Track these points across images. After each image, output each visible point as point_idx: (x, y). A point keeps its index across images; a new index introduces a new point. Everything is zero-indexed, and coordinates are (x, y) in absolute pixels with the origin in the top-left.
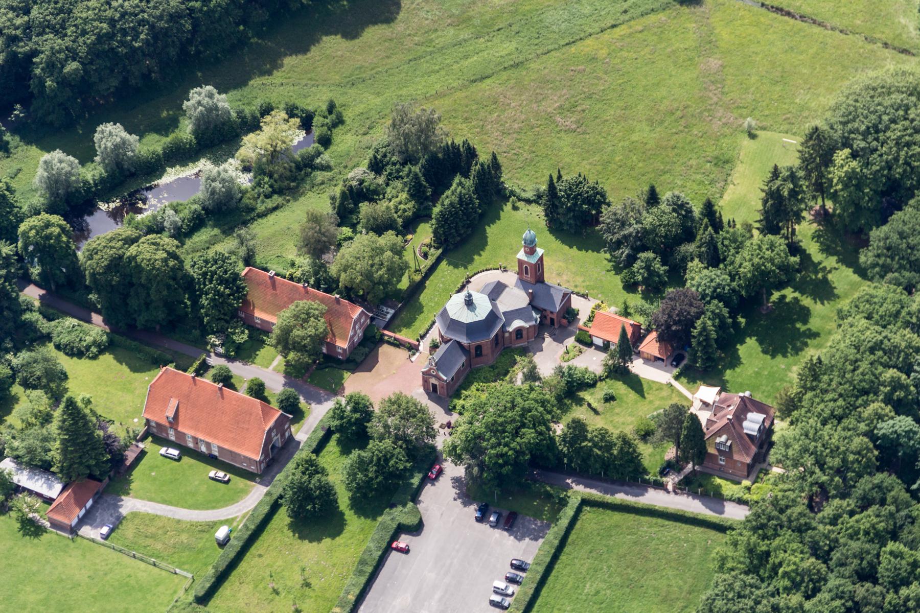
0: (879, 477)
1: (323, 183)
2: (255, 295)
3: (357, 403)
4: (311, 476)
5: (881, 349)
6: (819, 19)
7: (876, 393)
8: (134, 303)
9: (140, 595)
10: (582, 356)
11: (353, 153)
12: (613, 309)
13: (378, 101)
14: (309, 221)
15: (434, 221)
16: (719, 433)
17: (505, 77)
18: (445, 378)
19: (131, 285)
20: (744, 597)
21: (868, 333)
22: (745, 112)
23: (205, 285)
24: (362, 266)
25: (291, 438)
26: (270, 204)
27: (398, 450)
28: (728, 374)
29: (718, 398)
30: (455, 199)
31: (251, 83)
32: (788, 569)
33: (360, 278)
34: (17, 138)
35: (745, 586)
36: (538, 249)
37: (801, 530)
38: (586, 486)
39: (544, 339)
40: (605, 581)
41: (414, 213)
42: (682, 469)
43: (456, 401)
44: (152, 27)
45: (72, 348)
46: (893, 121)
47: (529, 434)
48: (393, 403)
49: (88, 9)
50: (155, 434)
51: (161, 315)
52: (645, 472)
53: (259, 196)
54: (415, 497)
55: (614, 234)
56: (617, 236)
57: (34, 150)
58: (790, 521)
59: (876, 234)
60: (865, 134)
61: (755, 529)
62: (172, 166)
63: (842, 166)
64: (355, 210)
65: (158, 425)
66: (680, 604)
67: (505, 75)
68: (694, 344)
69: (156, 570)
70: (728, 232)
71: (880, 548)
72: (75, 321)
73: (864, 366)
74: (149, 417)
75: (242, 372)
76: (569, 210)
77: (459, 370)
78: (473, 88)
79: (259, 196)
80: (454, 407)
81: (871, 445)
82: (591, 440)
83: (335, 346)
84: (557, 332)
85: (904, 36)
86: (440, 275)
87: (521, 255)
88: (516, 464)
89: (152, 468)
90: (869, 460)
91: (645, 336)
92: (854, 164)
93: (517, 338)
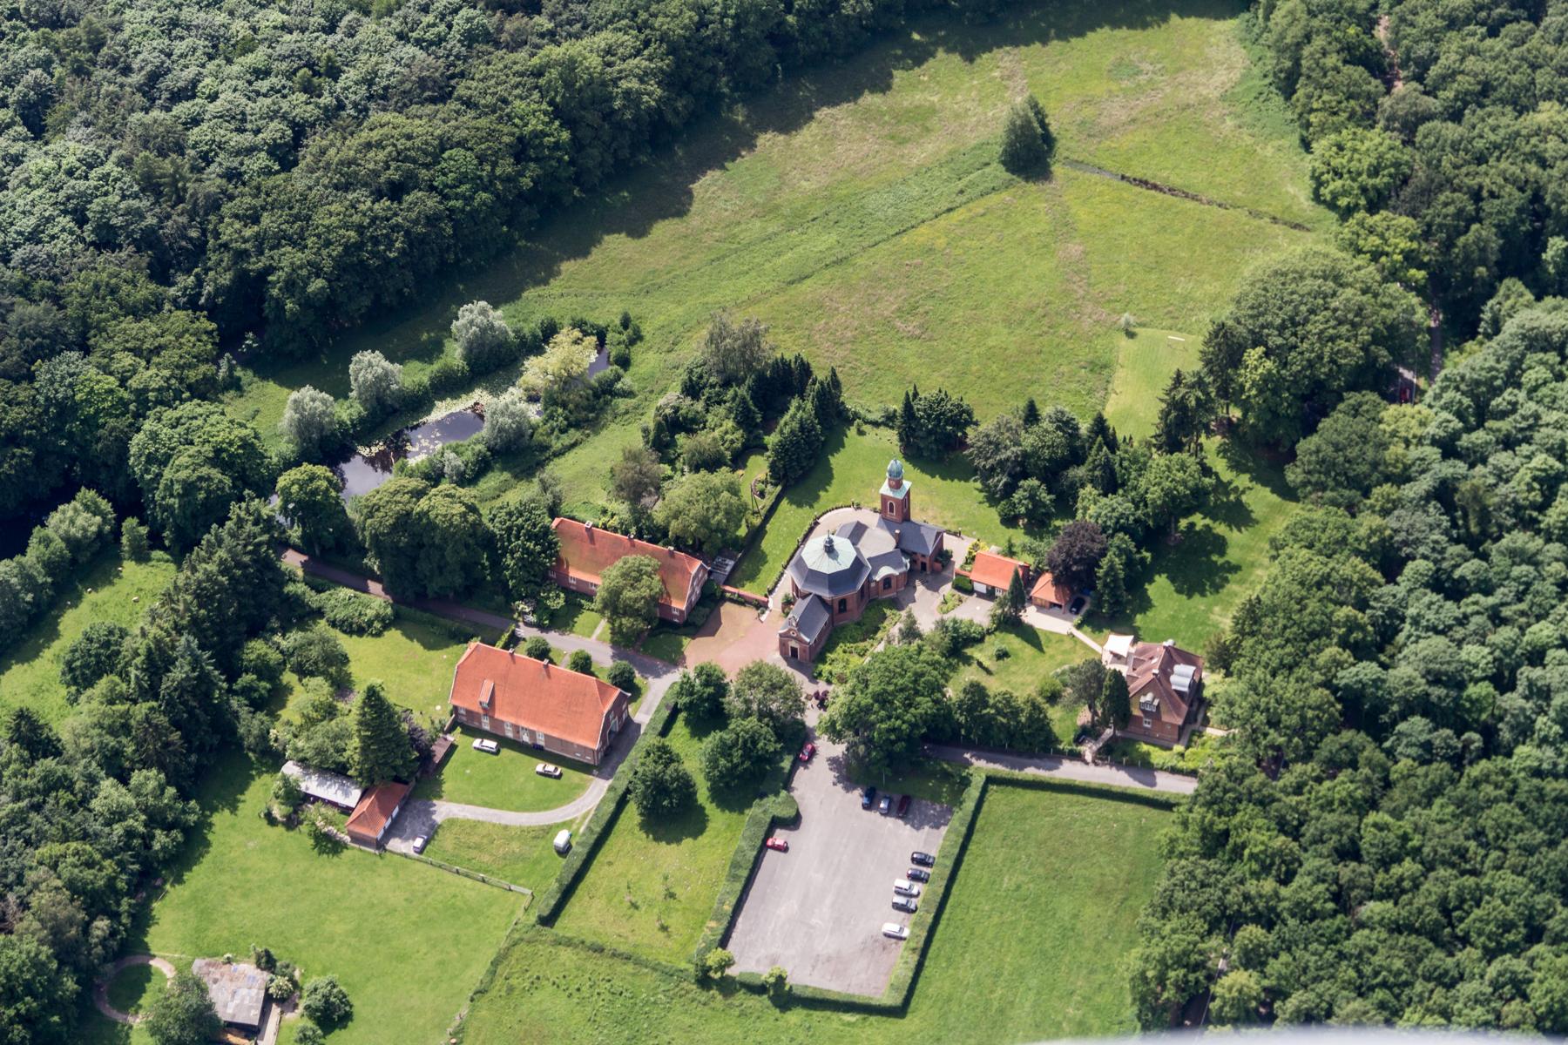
0: (1347, 735)
1: (627, 412)
2: (567, 550)
3: (709, 675)
4: (666, 765)
5: (1328, 582)
6: (1191, 192)
7: (1329, 636)
8: (424, 567)
9: (470, 919)
11: (658, 375)
12: (994, 548)
13: (680, 310)
14: (626, 459)
16: (1143, 691)
17: (828, 276)
19: (421, 546)
20: (1209, 885)
21: (1312, 565)
22: (1118, 306)
23: (510, 542)
24: (697, 510)
25: (629, 720)
26: (566, 440)
27: (765, 729)
28: (1139, 619)
29: (1133, 650)
30: (795, 425)
31: (525, 294)
32: (1256, 850)
34: (250, 373)
35: (1208, 873)
37: (1264, 803)
38: (989, 760)
40: (1025, 873)
42: (1099, 735)
43: (821, 667)
44: (408, 233)
45: (351, 625)
46: (1312, 312)
47: (925, 704)
48: (754, 674)
49: (331, 214)
50: (465, 723)
51: (458, 580)
52: (1058, 741)
53: (553, 430)
54: (787, 782)
55: (987, 459)
56: (991, 461)
57: (271, 387)
58: (1250, 793)
59: (1306, 445)
60: (1281, 329)
61: (1209, 804)
62: (442, 399)
63: (1256, 368)
64: (673, 443)
65: (469, 712)
66: (1119, 896)
67: (827, 274)
68: (1099, 587)
69: (486, 887)
70: (1126, 452)
71: (1361, 820)
72: (351, 592)
73: (1312, 605)
74: (457, 703)
75: (564, 644)
76: (930, 432)
78: (792, 290)
79: (553, 430)
80: (820, 674)
81: (1332, 699)
82: (994, 706)
83: (670, 608)
84: (930, 578)
85: (1295, 208)
87: (885, 489)
88: (909, 738)
89: (466, 765)
90: (1331, 716)
91: (1035, 579)
92: (1269, 364)
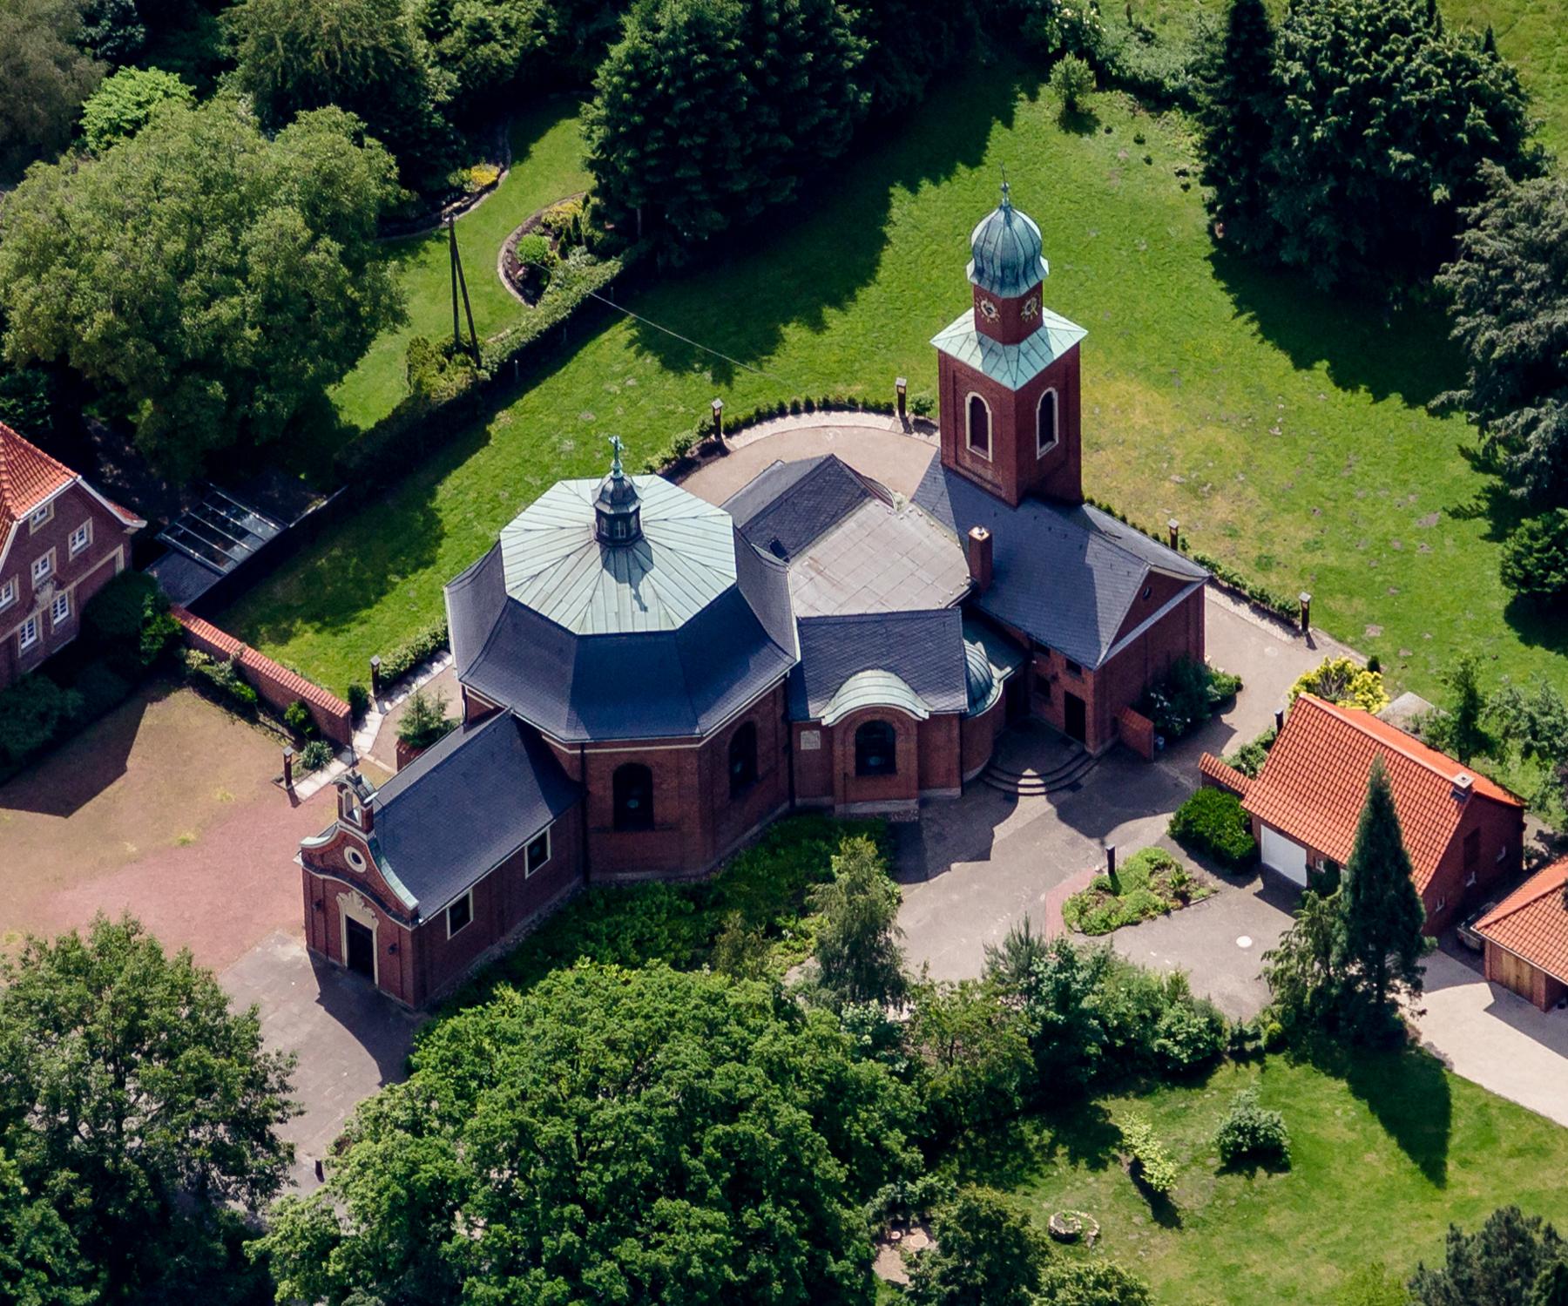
10: (1183, 920)
12: (1410, 704)
15: (596, 109)
18: (410, 901)
33: (102, 317)
36: (1050, 318)
39: (1012, 799)
41: (530, 56)
77: (510, 867)
86: (581, 392)
93: (862, 769)
